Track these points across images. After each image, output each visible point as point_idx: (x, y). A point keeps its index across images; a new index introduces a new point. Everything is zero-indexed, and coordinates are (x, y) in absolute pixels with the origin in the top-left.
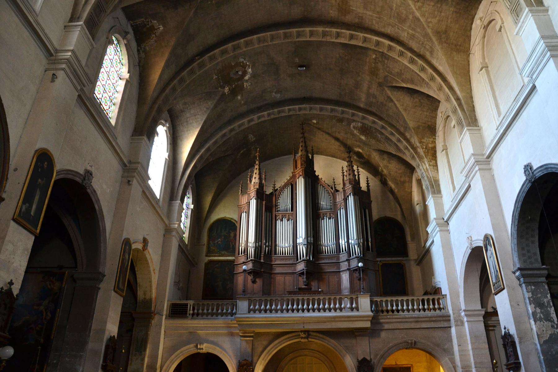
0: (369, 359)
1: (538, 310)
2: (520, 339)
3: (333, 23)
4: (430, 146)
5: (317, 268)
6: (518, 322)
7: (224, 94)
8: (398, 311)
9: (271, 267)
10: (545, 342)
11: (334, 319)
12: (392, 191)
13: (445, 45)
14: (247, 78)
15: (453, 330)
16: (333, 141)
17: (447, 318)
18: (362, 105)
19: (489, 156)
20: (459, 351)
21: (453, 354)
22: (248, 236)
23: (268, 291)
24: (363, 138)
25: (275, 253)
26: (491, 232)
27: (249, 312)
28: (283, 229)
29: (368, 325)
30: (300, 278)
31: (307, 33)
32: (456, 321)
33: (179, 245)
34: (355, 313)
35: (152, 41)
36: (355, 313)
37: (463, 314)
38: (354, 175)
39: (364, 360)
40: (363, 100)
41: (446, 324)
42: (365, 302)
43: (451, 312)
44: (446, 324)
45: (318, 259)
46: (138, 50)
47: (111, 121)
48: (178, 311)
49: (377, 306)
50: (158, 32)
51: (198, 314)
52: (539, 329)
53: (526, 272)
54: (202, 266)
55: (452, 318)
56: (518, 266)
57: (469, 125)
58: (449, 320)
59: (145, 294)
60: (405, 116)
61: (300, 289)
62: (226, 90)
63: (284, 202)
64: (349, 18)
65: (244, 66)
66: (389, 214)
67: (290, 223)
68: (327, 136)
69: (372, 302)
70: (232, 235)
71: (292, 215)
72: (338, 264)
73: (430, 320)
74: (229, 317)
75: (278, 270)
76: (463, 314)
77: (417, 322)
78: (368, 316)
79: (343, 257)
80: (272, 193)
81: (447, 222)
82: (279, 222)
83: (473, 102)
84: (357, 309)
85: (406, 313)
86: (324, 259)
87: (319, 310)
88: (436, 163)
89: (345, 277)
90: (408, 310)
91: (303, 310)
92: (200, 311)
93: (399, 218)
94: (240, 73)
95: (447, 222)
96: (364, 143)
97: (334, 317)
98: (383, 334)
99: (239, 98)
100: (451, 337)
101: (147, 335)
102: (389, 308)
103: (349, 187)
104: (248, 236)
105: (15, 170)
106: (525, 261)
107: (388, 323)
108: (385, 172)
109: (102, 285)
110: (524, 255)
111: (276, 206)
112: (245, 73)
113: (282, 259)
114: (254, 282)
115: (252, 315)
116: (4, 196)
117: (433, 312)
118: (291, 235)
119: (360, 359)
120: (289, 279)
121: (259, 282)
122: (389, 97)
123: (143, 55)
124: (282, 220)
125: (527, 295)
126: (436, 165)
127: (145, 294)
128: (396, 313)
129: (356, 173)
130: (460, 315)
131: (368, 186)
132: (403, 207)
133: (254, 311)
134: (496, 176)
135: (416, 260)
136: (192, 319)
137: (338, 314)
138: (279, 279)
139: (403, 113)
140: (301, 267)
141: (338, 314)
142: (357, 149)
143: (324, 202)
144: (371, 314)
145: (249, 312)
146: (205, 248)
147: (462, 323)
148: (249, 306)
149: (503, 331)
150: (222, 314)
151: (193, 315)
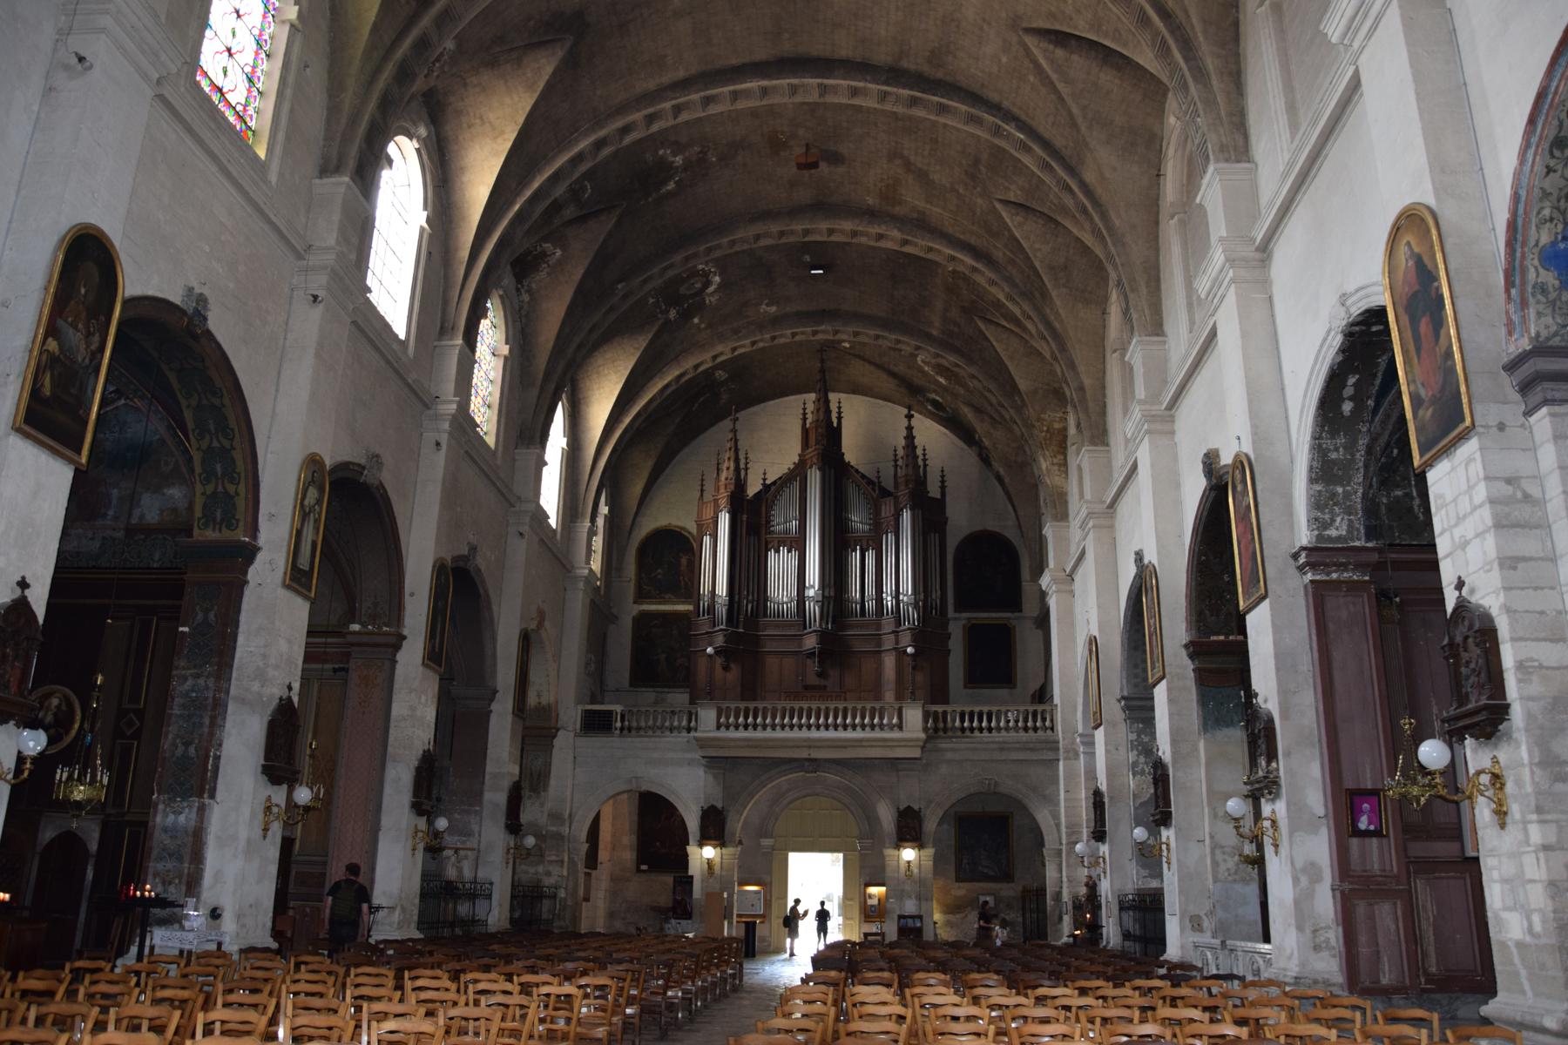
0: (916, 808)
2: (1111, 798)
3: (872, 214)
4: (1057, 426)
5: (841, 633)
7: (667, 321)
8: (972, 729)
11: (859, 743)
13: (1064, 290)
14: (711, 289)
17: (1053, 746)
21: (1058, 804)
23: (751, 689)
24: (942, 380)
25: (765, 615)
27: (718, 728)
28: (780, 565)
29: (916, 753)
30: (809, 662)
32: (1067, 751)
35: (543, 275)
36: (896, 734)
38: (916, 467)
40: (937, 324)
41: (1050, 756)
44: (1050, 756)
47: (486, 438)
48: (596, 723)
49: (936, 720)
50: (552, 261)
54: (627, 623)
59: (539, 696)
60: (1011, 368)
62: (673, 314)
63: (783, 520)
65: (706, 274)
66: (992, 526)
67: (795, 555)
69: (926, 715)
71: (798, 544)
72: (878, 639)
73: (1026, 747)
75: (770, 647)
77: (1002, 749)
78: (917, 740)
79: (888, 625)
81: (1070, 575)
82: (771, 554)
83: (1104, 396)
84: (900, 727)
85: (986, 733)
87: (836, 727)
90: (990, 730)
91: (809, 727)
92: (634, 724)
93: (1011, 534)
94: (698, 285)
95: (1070, 575)
97: (861, 740)
98: (944, 769)
99: (696, 321)
101: (548, 765)
103: (903, 493)
105: (412, 595)
106: (1136, 686)
107: (952, 750)
108: (987, 442)
111: (768, 522)
112: (708, 283)
113: (777, 626)
114: (726, 668)
115: (723, 734)
121: (735, 670)
122: (981, 331)
123: (526, 297)
126: (1065, 464)
127: (539, 696)
129: (920, 463)
130: (1074, 742)
132: (1021, 513)
137: (868, 734)
138: (772, 663)
139: (1008, 363)
140: (811, 642)
142: (933, 396)
143: (858, 520)
144: (923, 736)
145: (718, 728)
147: (1077, 755)
148: (719, 717)
149: (791, 904)
150: (671, 729)
151: (622, 729)
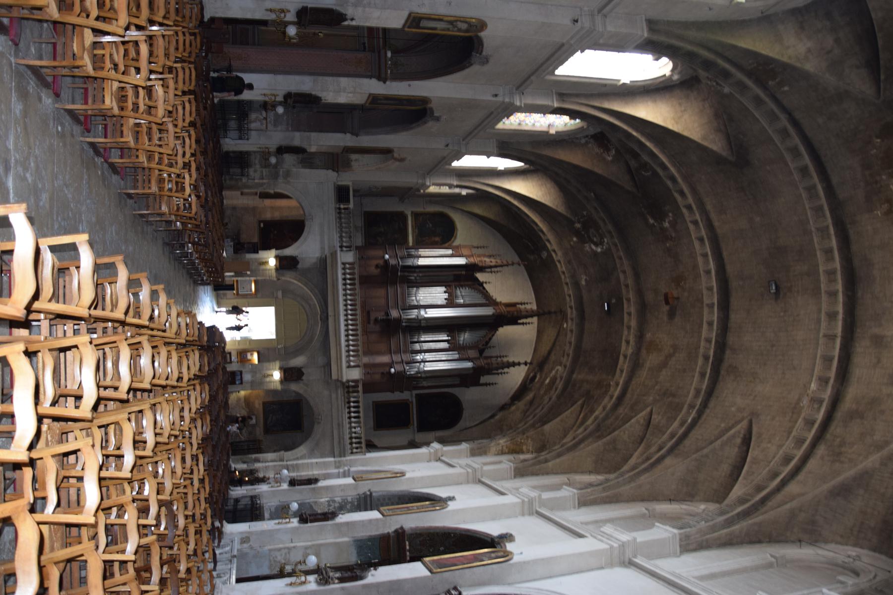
0: (304, 378)
1: (337, 505)
2: (314, 489)
3: (640, 337)
4: (524, 448)
6: (327, 488)
7: (574, 223)
8: (349, 407)
9: (394, 283)
10: (311, 507)
12: (492, 416)
14: (594, 247)
15: (332, 459)
16: (548, 348)
17: (342, 454)
18: (574, 376)
19: (481, 482)
20: (312, 463)
21: (309, 458)
22: (431, 258)
23: (366, 281)
26: (408, 475)
28: (438, 294)
30: (383, 313)
31: (631, 308)
32: (339, 462)
33: (411, 188)
34: (344, 365)
35: (597, 150)
36: (344, 365)
37: (346, 468)
39: (303, 374)
40: (579, 376)
41: (337, 452)
42: (355, 374)
43: (348, 458)
44: (337, 452)
45: (404, 333)
46: (587, 136)
47: (501, 123)
48: (342, 194)
51: (340, 213)
52: (321, 503)
53: (368, 499)
55: (343, 459)
56: (374, 494)
57: (515, 469)
58: (340, 456)
61: (368, 313)
62: (578, 225)
63: (463, 295)
64: (644, 352)
66: (466, 414)
68: (552, 341)
70: (437, 239)
72: (399, 351)
74: (339, 244)
75: (391, 290)
76: (346, 468)
77: (339, 425)
79: (406, 357)
80: (477, 279)
82: (443, 289)
83: (543, 474)
84: (349, 367)
86: (404, 337)
88: (505, 453)
89: (385, 359)
93: (462, 424)
94: (595, 239)
96: (543, 382)
97: (340, 344)
99: (575, 239)
100: (326, 457)
102: (352, 399)
104: (431, 258)
106: (378, 500)
108: (513, 408)
109: (348, 135)
110: (384, 499)
112: (596, 245)
113: (403, 294)
114: (377, 266)
115: (340, 266)
116: (388, 83)
117: (348, 436)
118: (432, 301)
119: (303, 370)
120: (382, 302)
122: (576, 402)
123: (583, 141)
124: (445, 292)
125: (349, 499)
127: (356, 160)
128: (347, 405)
129: (500, 371)
130: (345, 465)
131: (486, 384)
133: (344, 269)
134: (460, 486)
135: (414, 441)
136: (336, 208)
138: (381, 292)
140: (394, 314)
141: (344, 349)
144: (344, 380)
145: (344, 264)
146: (420, 209)
147: (338, 467)
148: (349, 264)
151: (340, 209)
